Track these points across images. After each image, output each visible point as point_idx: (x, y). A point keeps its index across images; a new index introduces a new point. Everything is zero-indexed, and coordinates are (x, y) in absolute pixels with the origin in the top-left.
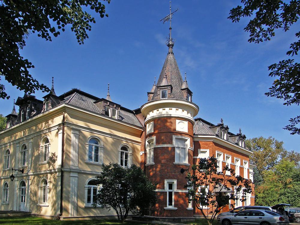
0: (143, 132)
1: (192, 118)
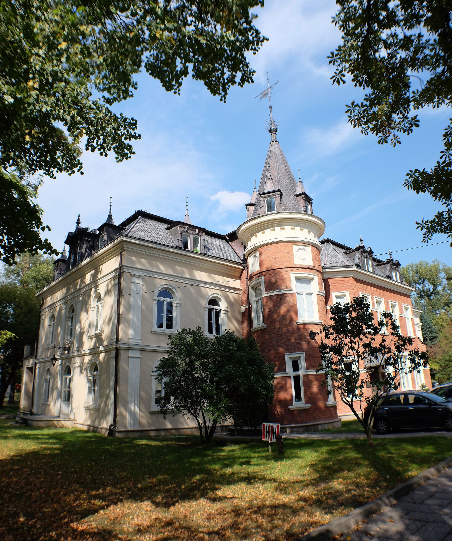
0: (243, 270)
1: (316, 239)
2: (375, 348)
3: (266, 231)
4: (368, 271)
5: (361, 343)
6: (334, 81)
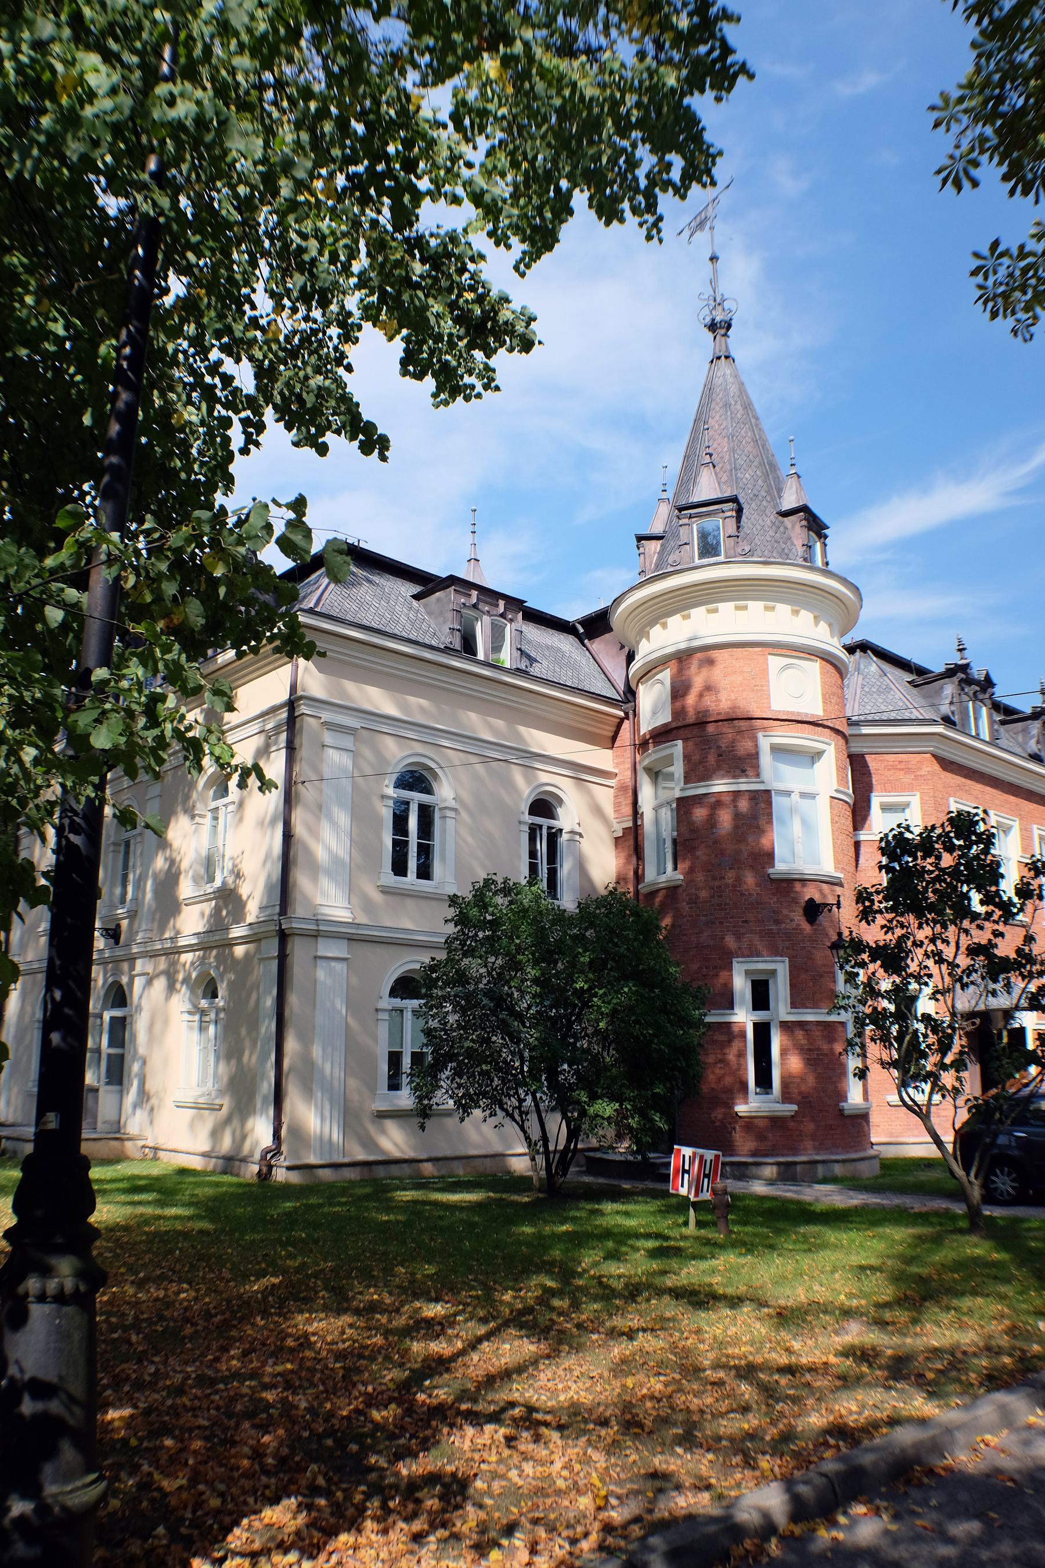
0: (621, 721)
1: (835, 641)
2: (1006, 959)
3: (693, 612)
4: (977, 737)
5: (965, 942)
6: (945, 181)
